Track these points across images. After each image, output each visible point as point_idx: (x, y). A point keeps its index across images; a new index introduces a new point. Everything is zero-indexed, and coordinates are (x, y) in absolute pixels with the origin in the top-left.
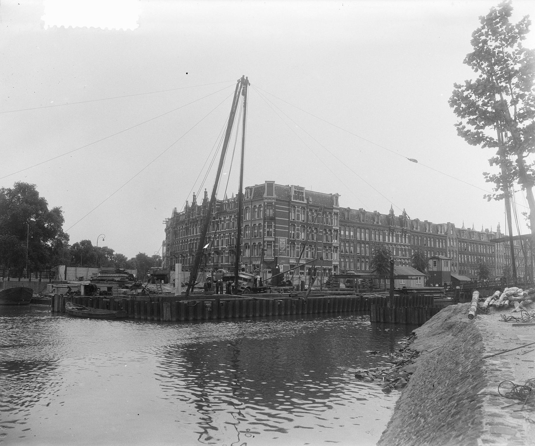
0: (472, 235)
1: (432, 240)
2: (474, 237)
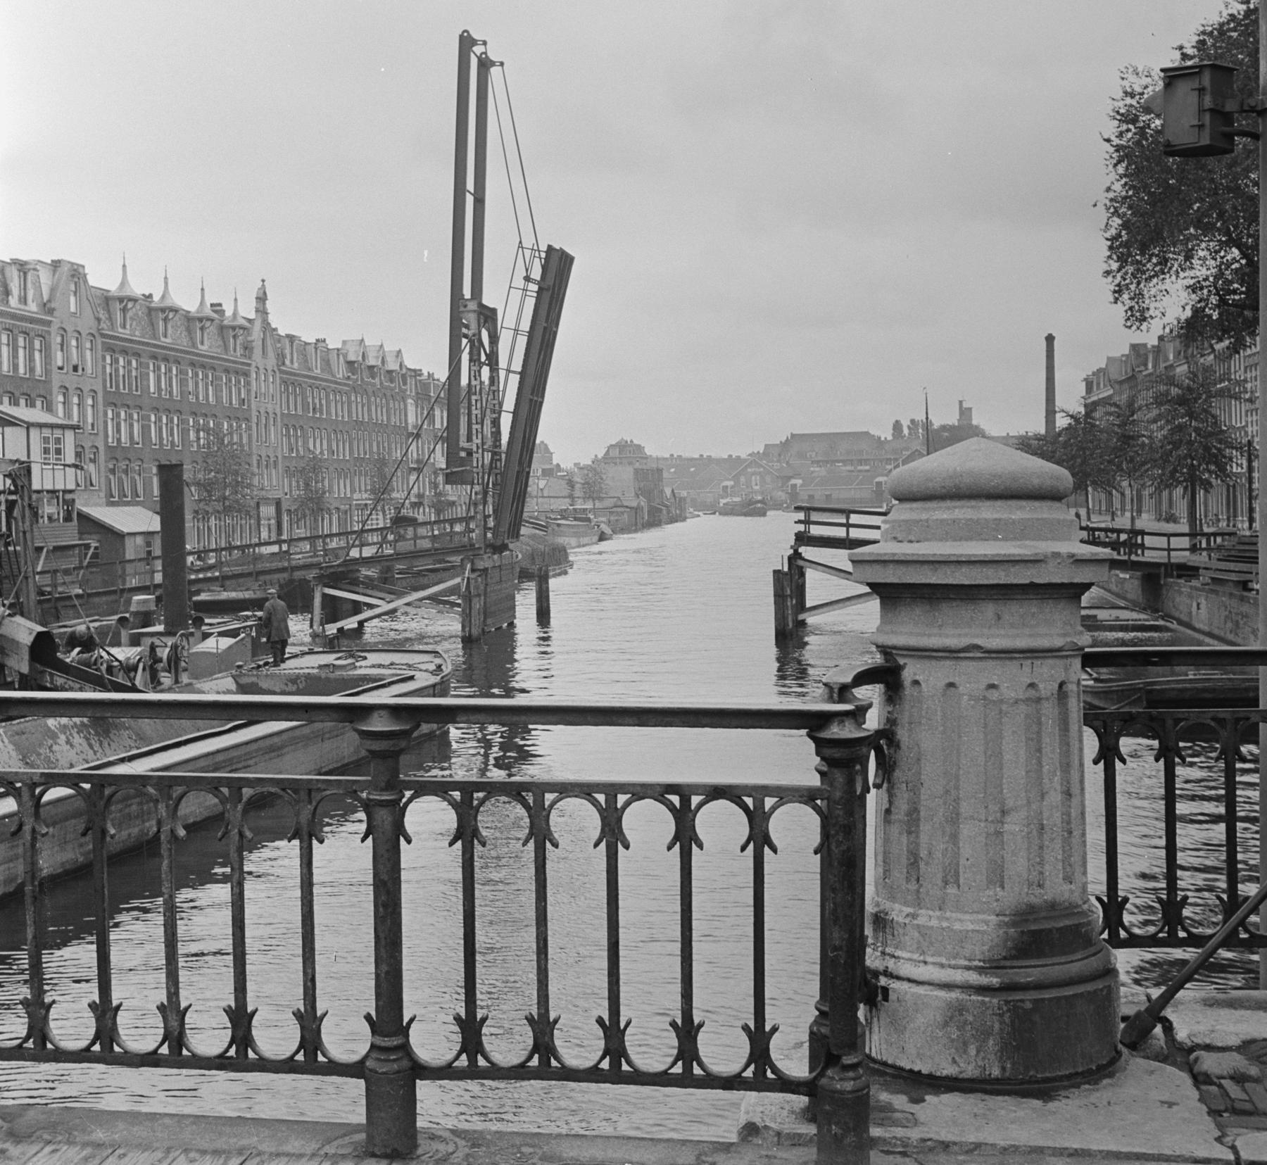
2: (170, 331)
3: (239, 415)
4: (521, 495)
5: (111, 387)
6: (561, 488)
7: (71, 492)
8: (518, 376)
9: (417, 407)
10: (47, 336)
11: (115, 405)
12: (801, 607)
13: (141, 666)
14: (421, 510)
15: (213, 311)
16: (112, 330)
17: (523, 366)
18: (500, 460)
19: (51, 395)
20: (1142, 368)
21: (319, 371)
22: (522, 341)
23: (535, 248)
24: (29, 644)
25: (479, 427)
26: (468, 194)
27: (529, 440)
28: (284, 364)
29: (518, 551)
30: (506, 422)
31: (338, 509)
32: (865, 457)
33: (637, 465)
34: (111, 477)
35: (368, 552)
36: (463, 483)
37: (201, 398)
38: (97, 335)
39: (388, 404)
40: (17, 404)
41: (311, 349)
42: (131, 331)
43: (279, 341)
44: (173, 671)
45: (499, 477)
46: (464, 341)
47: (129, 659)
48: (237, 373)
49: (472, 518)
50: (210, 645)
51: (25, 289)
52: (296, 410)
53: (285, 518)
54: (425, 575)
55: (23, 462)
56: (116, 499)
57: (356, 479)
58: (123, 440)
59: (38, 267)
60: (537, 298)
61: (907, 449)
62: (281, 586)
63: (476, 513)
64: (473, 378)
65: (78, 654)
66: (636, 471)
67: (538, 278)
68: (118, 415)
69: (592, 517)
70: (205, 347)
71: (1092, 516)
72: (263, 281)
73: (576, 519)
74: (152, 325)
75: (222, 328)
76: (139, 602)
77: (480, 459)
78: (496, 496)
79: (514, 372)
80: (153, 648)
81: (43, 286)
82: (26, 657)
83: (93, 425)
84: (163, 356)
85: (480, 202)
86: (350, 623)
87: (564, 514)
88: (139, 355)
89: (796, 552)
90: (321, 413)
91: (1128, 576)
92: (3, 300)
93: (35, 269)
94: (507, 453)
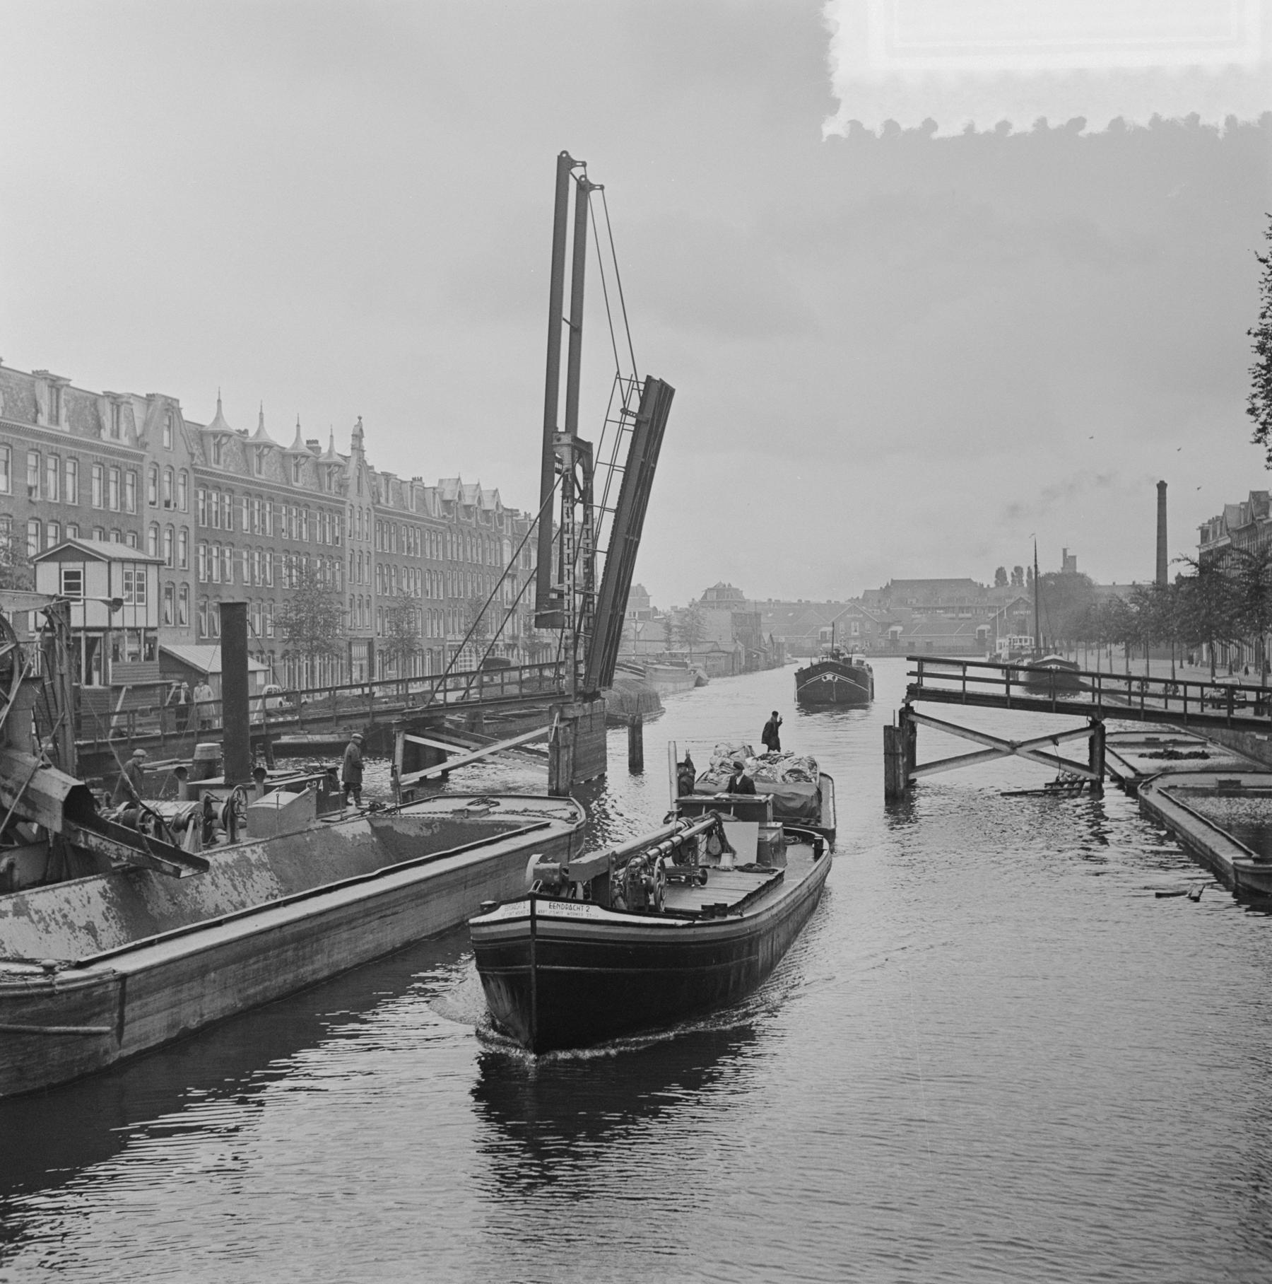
0: (255, 460)
1: (70, 467)
2: (264, 468)
3: (332, 554)
4: (614, 639)
5: (204, 523)
6: (658, 631)
7: (153, 629)
8: (613, 514)
9: (513, 547)
10: (139, 471)
11: (207, 542)
12: (912, 766)
13: (191, 823)
14: (515, 652)
15: (310, 448)
16: (206, 465)
17: (619, 503)
18: (593, 603)
19: (142, 529)
20: (1263, 516)
21: (414, 510)
22: (618, 478)
23: (634, 379)
24: (63, 800)
25: (570, 567)
26: (563, 322)
27: (623, 584)
28: (379, 502)
29: (609, 696)
30: (600, 561)
31: (431, 650)
32: (967, 604)
33: (735, 610)
34: (202, 614)
35: (452, 697)
36: (554, 626)
37: (294, 536)
38: (190, 470)
39: (464, 540)
40: (107, 539)
41: (407, 488)
42: (225, 467)
43: (375, 479)
44: (229, 829)
45: (591, 620)
46: (557, 476)
47: (178, 815)
48: (331, 510)
49: (562, 664)
50: (270, 800)
51: (118, 422)
52: (383, 548)
53: (377, 658)
54: (511, 721)
55: (61, 599)
56: (207, 637)
57: (450, 620)
58: (214, 577)
59: (132, 401)
60: (634, 432)
61: (1010, 597)
62: (366, 730)
63: (566, 658)
64: (565, 516)
65: (125, 809)
66: (734, 615)
67: (636, 411)
68: (210, 552)
69: (689, 662)
70: (299, 484)
71: (1217, 671)
72: (360, 418)
73: (672, 664)
74: (247, 461)
75: (317, 465)
76: (202, 750)
77: (572, 601)
78: (588, 640)
79: (610, 510)
80: (208, 803)
81: (136, 420)
82: (59, 814)
83: (184, 561)
84: (254, 493)
85: (576, 331)
86: (434, 772)
87: (659, 658)
88: (233, 492)
89: (907, 705)
90: (416, 553)
91: (1266, 738)
92: (95, 433)
93: (128, 403)
94: (599, 595)
